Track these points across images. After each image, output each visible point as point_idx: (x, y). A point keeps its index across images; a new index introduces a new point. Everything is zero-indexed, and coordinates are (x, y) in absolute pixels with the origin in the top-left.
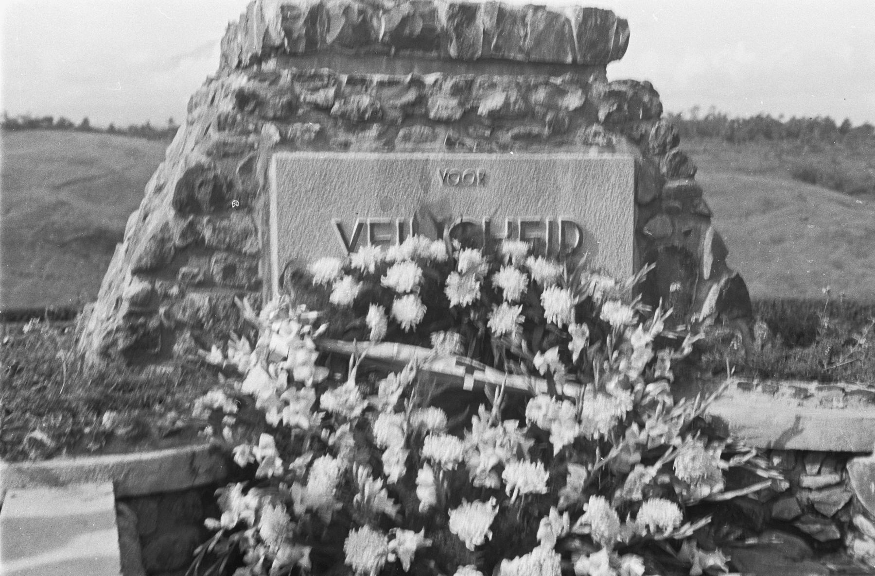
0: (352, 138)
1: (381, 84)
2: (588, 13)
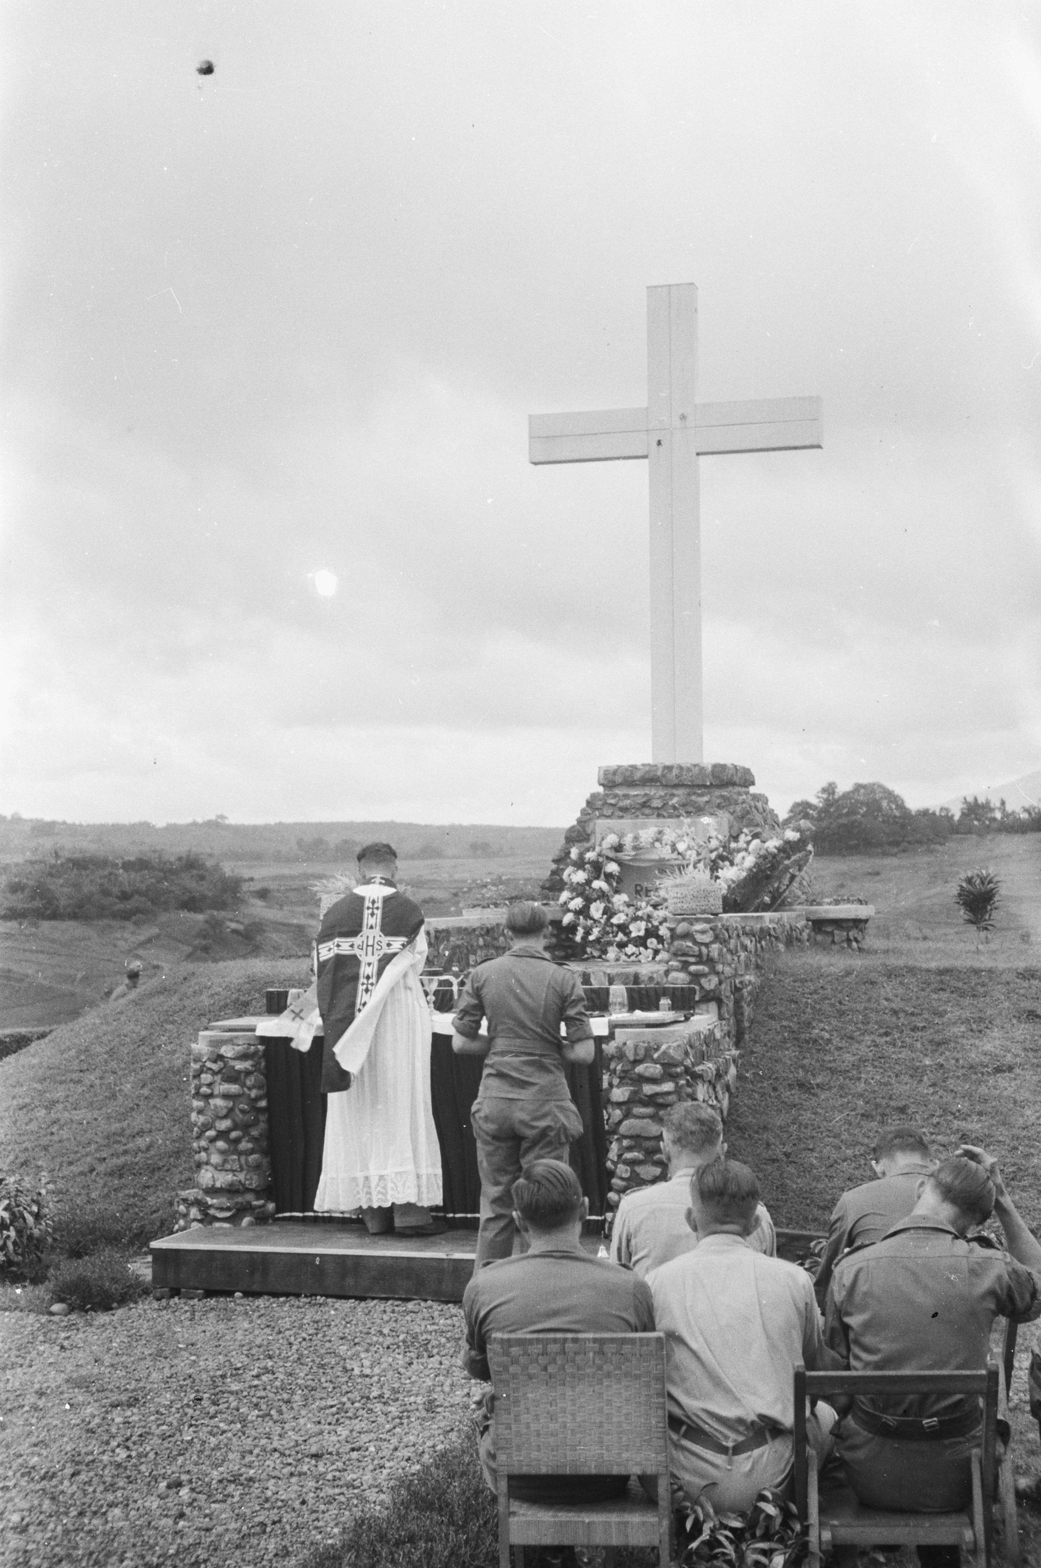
2: (715, 766)
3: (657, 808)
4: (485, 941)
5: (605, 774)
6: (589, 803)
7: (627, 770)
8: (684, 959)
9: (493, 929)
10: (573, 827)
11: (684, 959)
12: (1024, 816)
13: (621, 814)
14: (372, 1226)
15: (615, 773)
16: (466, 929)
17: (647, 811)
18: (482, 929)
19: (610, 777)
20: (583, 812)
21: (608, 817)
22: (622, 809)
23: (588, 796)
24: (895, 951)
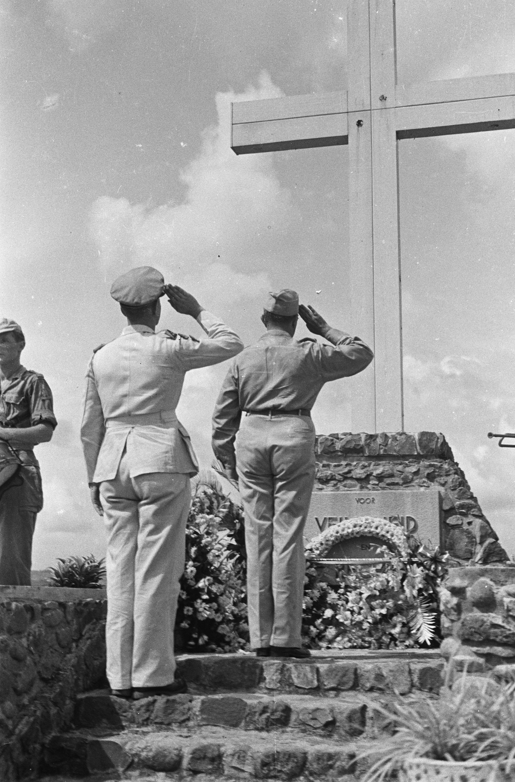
0: (324, 487)
7: (327, 439)
8: (486, 650)
11: (486, 650)
13: (321, 486)
17: (349, 482)
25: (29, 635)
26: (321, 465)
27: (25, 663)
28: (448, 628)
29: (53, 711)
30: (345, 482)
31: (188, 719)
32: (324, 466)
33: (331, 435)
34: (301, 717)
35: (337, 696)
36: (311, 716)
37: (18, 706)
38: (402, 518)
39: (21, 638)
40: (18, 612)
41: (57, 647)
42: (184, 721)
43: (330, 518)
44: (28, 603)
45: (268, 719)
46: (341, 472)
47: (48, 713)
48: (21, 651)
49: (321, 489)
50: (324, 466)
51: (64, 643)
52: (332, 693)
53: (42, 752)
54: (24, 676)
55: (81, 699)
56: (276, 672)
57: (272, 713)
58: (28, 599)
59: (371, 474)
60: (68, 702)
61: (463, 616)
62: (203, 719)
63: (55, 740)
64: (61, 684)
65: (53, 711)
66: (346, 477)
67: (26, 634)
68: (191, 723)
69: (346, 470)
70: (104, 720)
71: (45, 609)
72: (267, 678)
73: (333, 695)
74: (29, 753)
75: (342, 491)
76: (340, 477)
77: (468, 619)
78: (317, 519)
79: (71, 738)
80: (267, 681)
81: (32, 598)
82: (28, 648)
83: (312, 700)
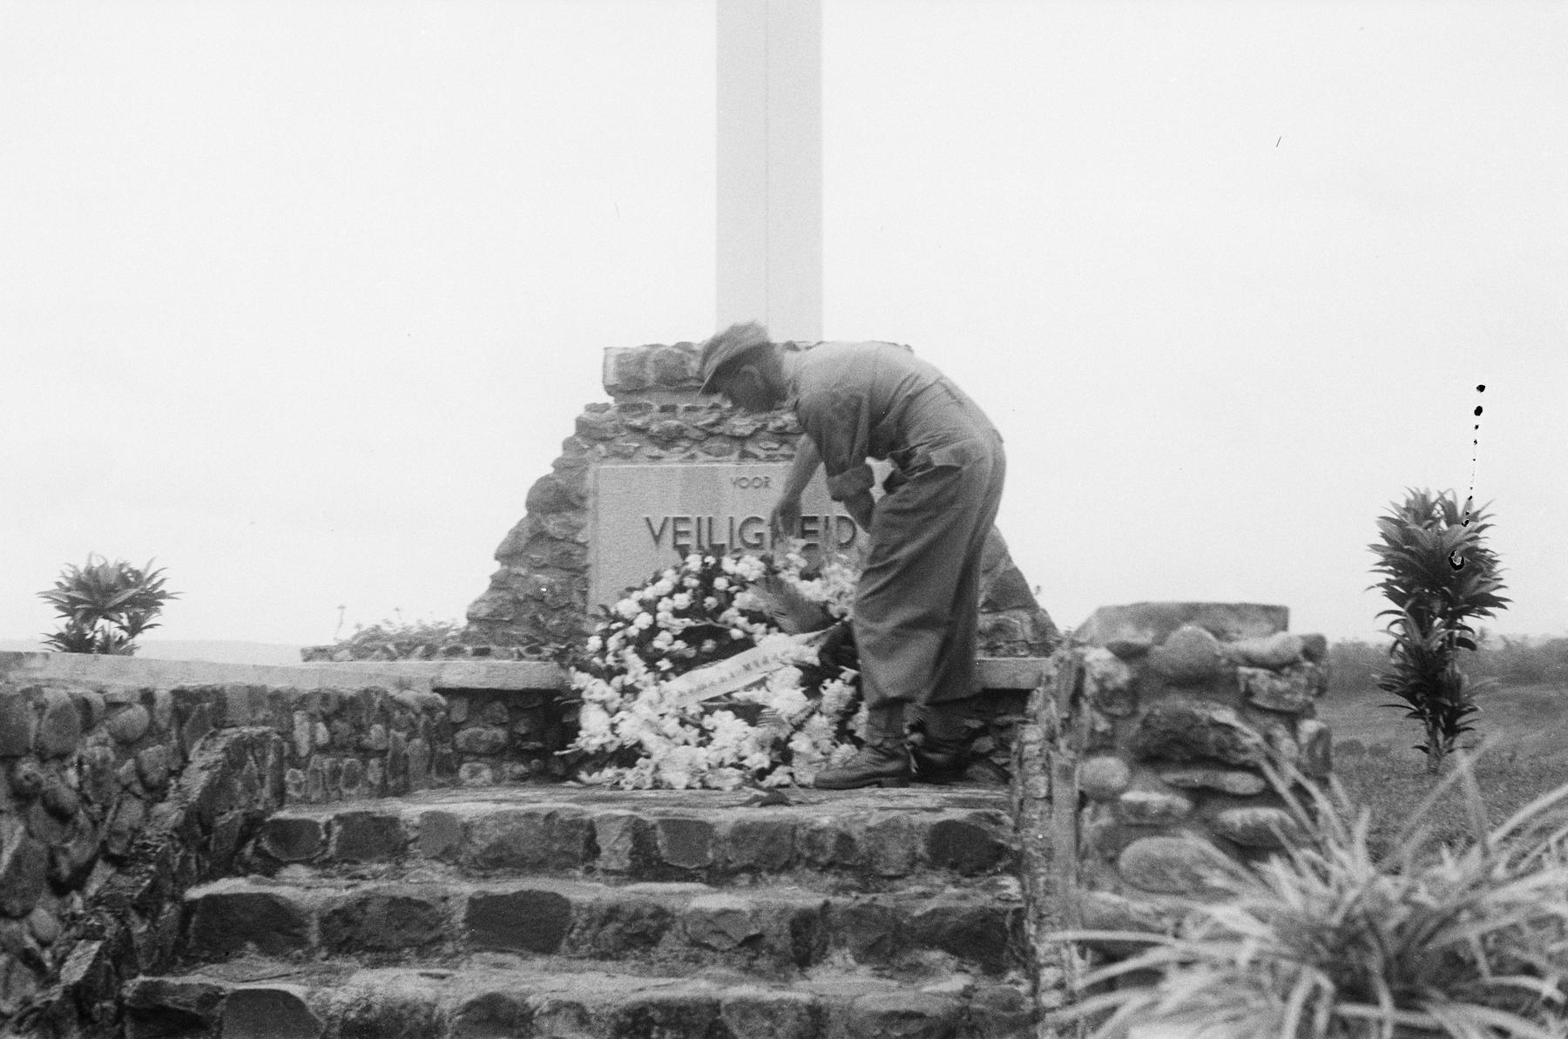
0: (663, 453)
1: (688, 409)
3: (742, 439)
4: (333, 734)
5: (619, 364)
6: (583, 426)
7: (669, 353)
8: (1197, 777)
9: (353, 700)
10: (547, 478)
11: (1197, 777)
12: (1170, 672)
13: (656, 451)
14: (704, 875)
15: (642, 360)
16: (276, 696)
17: (715, 444)
18: (325, 698)
19: (633, 370)
20: (568, 445)
21: (627, 457)
22: (654, 439)
23: (580, 411)
24: (577, 801)
25: (80, 763)
26: (657, 407)
27: (76, 823)
28: (1103, 734)
29: (140, 928)
30: (707, 444)
31: (440, 939)
32: (664, 409)
33: (678, 346)
34: (689, 929)
35: (754, 882)
36: (710, 927)
37: (61, 918)
38: (699, 519)
39: (65, 768)
40: (61, 714)
41: (138, 788)
42: (432, 942)
43: (676, 519)
44: (78, 691)
45: (619, 932)
46: (700, 424)
47: (128, 930)
48: (68, 798)
49: (659, 458)
50: (664, 409)
51: (154, 777)
52: (744, 879)
53: (118, 1018)
54: (75, 852)
55: (194, 902)
56: (621, 835)
57: (628, 924)
58: (75, 682)
59: (764, 427)
60: (167, 907)
61: (1144, 710)
62: (472, 938)
63: (145, 991)
64: (152, 867)
65: (140, 928)
66: (709, 433)
67: (75, 759)
68: (448, 948)
69: (711, 419)
70: (250, 945)
71: (114, 705)
72: (603, 848)
73: (746, 882)
74: (93, 1022)
75: (702, 463)
76: (698, 433)
77: (1157, 712)
78: (731, 519)
79: (183, 987)
80: (604, 853)
81: (84, 679)
82: (79, 790)
83: (704, 893)
